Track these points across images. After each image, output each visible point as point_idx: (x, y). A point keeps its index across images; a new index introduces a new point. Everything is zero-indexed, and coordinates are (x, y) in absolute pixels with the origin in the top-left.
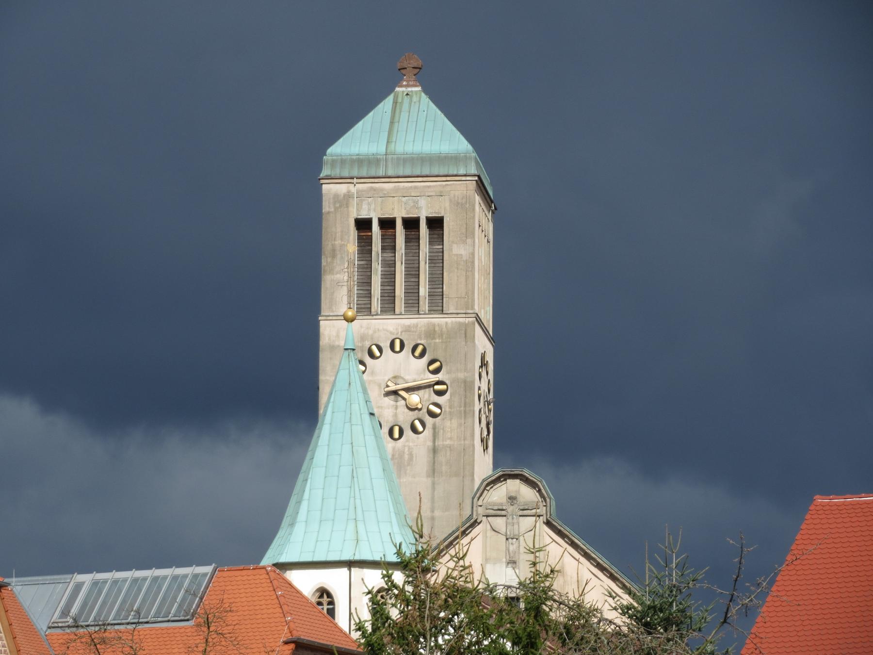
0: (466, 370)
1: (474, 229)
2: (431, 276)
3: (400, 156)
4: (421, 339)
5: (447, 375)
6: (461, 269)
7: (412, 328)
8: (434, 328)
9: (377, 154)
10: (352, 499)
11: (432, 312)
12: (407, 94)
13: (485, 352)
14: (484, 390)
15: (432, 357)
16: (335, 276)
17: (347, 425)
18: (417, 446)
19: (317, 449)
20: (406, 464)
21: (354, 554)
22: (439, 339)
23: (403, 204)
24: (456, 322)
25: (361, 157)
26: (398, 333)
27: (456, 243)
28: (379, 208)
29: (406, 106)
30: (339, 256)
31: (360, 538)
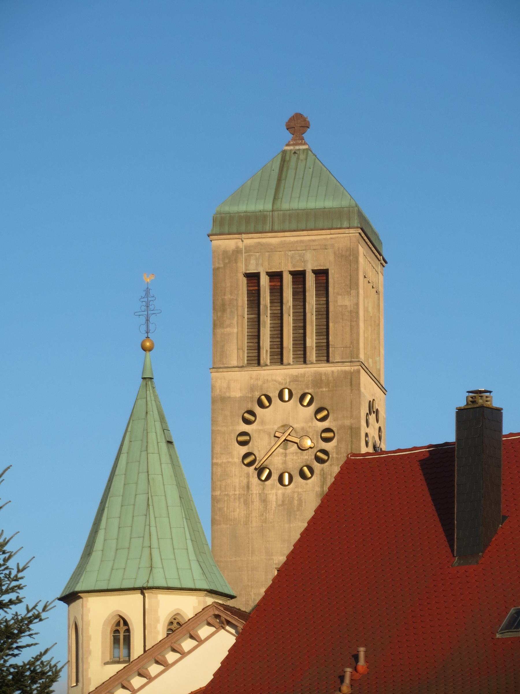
0: (351, 417)
1: (358, 280)
2: (318, 327)
3: (286, 212)
4: (308, 389)
5: (334, 422)
6: (346, 319)
7: (300, 378)
8: (321, 377)
9: (264, 211)
10: (147, 527)
11: (319, 362)
12: (295, 153)
13: (374, 400)
14: (374, 437)
15: (319, 406)
16: (225, 330)
17: (144, 454)
18: (305, 491)
19: (114, 478)
20: (295, 509)
21: (148, 582)
22: (326, 388)
23: (290, 259)
24: (342, 371)
25: (249, 214)
26: (286, 383)
27: (341, 295)
28: (267, 263)
29: (293, 164)
30: (228, 310)
31: (154, 565)
